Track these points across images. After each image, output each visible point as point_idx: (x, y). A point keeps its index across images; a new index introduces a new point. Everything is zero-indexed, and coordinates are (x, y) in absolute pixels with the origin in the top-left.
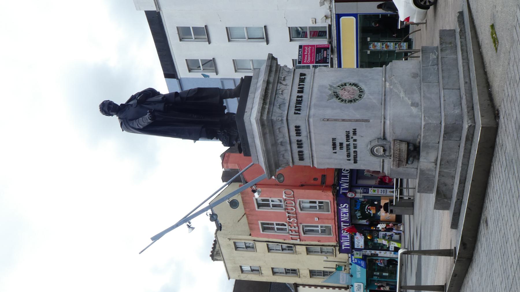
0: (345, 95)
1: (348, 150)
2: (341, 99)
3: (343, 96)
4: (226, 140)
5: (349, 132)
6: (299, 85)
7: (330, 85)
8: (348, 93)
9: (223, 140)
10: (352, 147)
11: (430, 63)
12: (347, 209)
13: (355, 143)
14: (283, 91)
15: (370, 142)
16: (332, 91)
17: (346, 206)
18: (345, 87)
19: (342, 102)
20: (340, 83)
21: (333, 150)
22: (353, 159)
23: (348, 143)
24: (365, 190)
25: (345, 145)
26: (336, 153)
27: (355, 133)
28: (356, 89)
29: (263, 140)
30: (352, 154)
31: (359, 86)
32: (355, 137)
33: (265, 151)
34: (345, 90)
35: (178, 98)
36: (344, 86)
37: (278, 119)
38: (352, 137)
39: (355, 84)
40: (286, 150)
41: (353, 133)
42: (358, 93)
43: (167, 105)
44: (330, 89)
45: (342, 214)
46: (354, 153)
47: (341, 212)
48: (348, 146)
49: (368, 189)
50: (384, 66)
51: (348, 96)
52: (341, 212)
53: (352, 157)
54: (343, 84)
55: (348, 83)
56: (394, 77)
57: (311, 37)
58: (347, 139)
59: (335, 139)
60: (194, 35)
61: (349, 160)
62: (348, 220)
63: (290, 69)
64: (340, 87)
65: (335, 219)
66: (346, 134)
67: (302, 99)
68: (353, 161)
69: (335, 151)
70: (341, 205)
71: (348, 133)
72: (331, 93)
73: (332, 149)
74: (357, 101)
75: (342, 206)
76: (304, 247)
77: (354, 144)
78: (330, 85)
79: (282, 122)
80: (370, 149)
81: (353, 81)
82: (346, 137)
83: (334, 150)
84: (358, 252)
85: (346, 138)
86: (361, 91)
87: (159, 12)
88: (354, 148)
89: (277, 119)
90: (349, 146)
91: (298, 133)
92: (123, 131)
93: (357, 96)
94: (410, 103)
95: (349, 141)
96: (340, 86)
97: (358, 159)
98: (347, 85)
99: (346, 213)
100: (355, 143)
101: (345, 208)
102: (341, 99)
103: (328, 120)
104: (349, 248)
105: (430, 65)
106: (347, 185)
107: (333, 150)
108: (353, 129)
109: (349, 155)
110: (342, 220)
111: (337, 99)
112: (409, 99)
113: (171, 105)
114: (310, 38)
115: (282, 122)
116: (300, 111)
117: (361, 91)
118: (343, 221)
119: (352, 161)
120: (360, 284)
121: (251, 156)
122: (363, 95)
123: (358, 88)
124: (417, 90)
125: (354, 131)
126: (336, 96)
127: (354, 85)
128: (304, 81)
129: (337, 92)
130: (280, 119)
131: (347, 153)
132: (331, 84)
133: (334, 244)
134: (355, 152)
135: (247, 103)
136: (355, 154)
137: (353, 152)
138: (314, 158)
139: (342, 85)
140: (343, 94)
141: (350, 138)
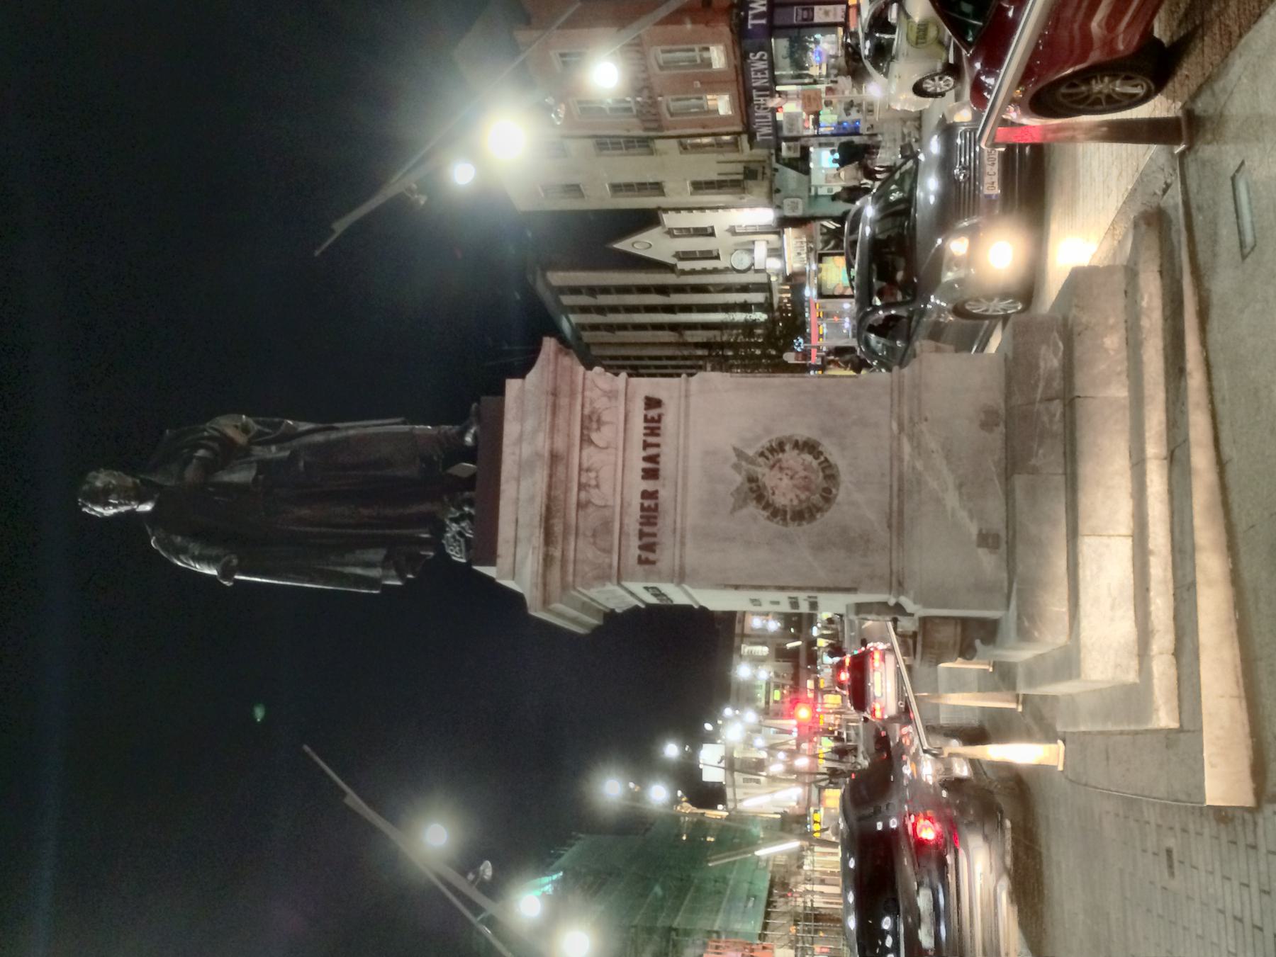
0: (784, 491)
3: (777, 492)
6: (646, 445)
7: (735, 449)
11: (1040, 390)
12: (766, 62)
16: (744, 473)
17: (763, 55)
18: (781, 455)
19: (775, 520)
20: (765, 442)
24: (805, 13)
28: (815, 463)
34: (781, 469)
36: (776, 451)
42: (819, 479)
44: (736, 467)
45: (753, 73)
47: (752, 69)
49: (813, 10)
51: (792, 495)
52: (752, 69)
54: (774, 445)
55: (789, 439)
56: (925, 423)
62: (767, 84)
65: (737, 80)
67: (657, 505)
70: (751, 55)
72: (742, 484)
75: (754, 56)
76: (674, 142)
78: (735, 449)
81: (802, 433)
84: (791, 144)
86: (829, 471)
93: (818, 496)
94: (973, 529)
96: (767, 453)
98: (787, 447)
99: (762, 72)
101: (761, 59)
104: (771, 137)
105: (1038, 397)
106: (764, 5)
110: (754, 85)
112: (971, 517)
116: (654, 551)
117: (828, 472)
118: (755, 88)
120: (796, 200)
122: (834, 491)
123: (819, 461)
124: (997, 482)
127: (806, 450)
128: (659, 428)
132: (739, 445)
133: (738, 128)
139: (772, 450)
140: (776, 487)
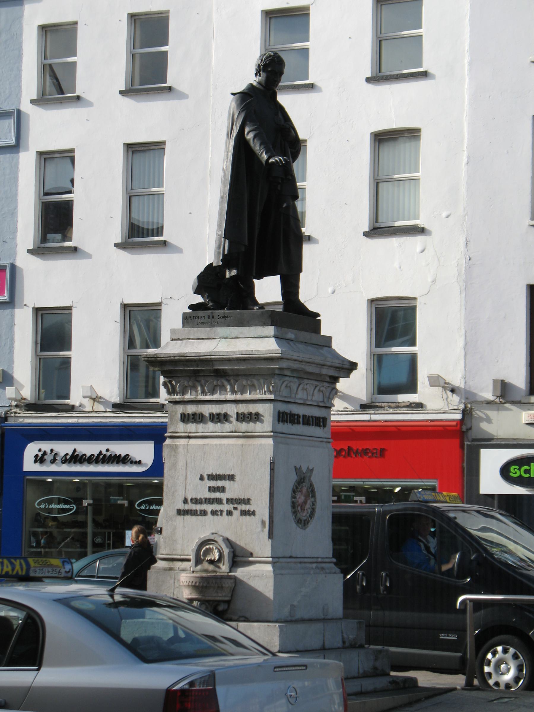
23: (225, 501)
25: (217, 495)
26: (202, 478)
27: (244, 513)
30: (198, 507)
32: (236, 513)
33: (210, 359)
48: (219, 501)
50: (334, 560)
55: (315, 501)
57: (129, 357)
60: (142, 54)
63: (332, 400)
64: (310, 487)
68: (182, 508)
69: (206, 477)
91: (242, 417)
97: (188, 518)
98: (313, 500)
102: (297, 490)
109: (196, 501)
114: (128, 356)
119: (181, 506)
122: (300, 526)
127: (312, 510)
134: (204, 513)
136: (199, 513)
141: (236, 506)
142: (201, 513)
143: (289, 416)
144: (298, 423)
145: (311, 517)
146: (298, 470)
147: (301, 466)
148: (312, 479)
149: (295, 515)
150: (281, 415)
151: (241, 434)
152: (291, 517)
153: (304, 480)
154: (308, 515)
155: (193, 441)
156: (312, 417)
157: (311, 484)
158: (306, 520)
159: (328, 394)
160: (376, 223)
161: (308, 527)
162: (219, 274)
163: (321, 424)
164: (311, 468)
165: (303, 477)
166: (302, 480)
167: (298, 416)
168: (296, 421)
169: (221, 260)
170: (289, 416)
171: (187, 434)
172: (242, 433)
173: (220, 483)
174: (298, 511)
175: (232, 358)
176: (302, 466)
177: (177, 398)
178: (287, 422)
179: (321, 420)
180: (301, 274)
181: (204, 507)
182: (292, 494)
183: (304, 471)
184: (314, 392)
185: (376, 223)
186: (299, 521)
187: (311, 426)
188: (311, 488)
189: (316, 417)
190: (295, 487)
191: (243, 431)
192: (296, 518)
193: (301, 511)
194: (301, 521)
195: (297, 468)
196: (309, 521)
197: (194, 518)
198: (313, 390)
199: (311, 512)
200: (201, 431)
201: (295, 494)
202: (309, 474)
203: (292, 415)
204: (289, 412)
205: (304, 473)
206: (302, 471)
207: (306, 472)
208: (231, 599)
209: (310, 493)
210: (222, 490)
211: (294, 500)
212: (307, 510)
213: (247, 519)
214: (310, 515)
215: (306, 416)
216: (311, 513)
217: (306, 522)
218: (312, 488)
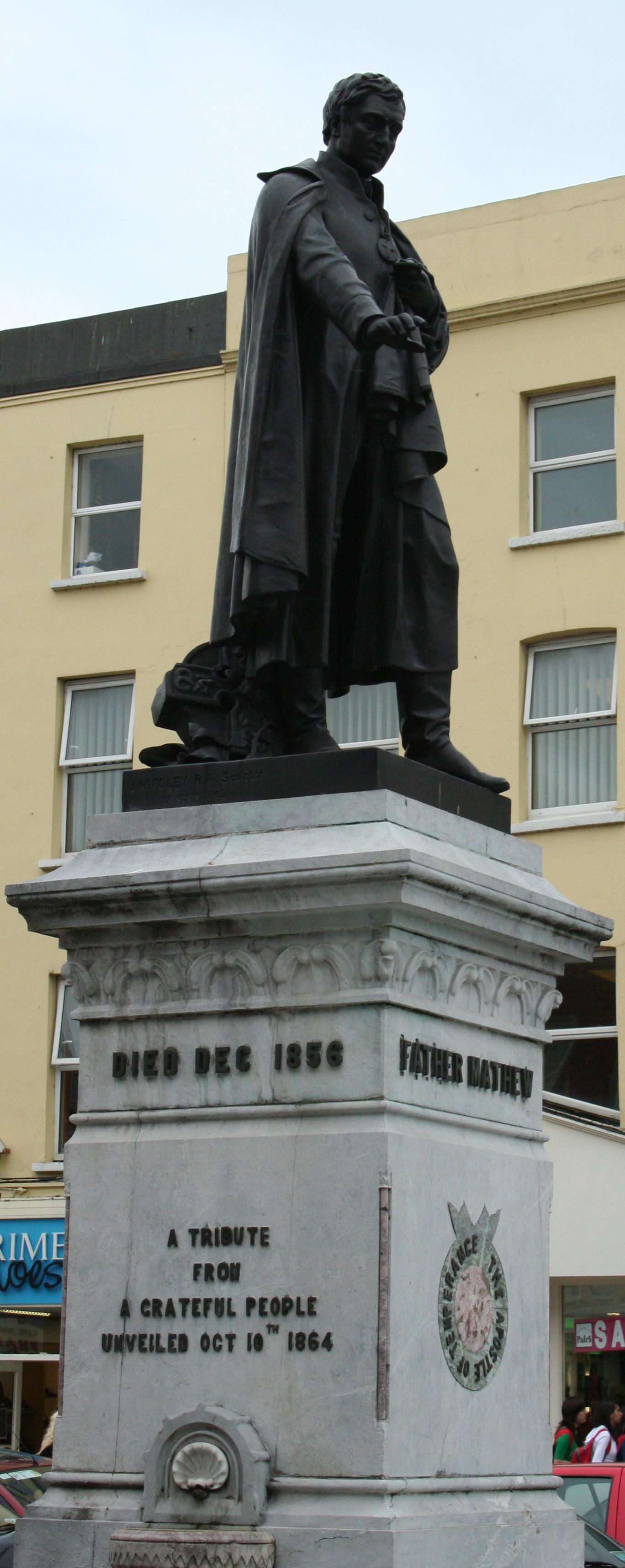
1: (195, 1308)
2: (452, 1275)
4: (197, 687)
5: (312, 1313)
8: (472, 1308)
9: (194, 669)
10: (212, 1325)
13: (241, 1343)
14: (519, 997)
15: (247, 1418)
18: (493, 1292)
21: (193, 1232)
22: (130, 1332)
23: (239, 1307)
25: (221, 1290)
26: (173, 1241)
29: (273, 881)
30: (164, 1328)
31: (494, 1361)
32: (275, 1344)
35: (417, 469)
37: (386, 961)
38: (281, 1329)
39: (502, 1341)
40: (184, 991)
41: (308, 1334)
43: (395, 408)
46: (172, 1337)
48: (222, 1308)
53: (137, 1325)
58: (263, 1301)
59: (264, 1244)
60: (93, 518)
61: (125, 1312)
66: (299, 1299)
69: (184, 1238)
71: (304, 1308)
73: (200, 1226)
74: (448, 1355)
77: (231, 1337)
79: (370, 980)
80: (215, 1417)
82: (275, 1300)
83: (189, 1238)
85: (270, 1298)
87: (219, 362)
88: (205, 1337)
89: (390, 957)
90: (219, 1314)
92: (264, 177)
95: (248, 1314)
97: (133, 1359)
98: (498, 1303)
100: (241, 1343)
102: (455, 1275)
103: (384, 1209)
107: (193, 1232)
108: (329, 1335)
111: (455, 1253)
113: (393, 429)
115: (370, 980)
119: (115, 1327)
121: (126, 807)
125: (320, 1339)
126: (463, 1247)
127: (497, 1334)
129: (475, 1252)
130: (388, 971)
131: (170, 1302)
134: (182, 1344)
135: (326, 795)
137: (177, 1331)
138: (132, 1129)
141: (271, 1320)
142: (171, 1344)
143: (430, 1054)
144: (457, 1078)
145: (495, 1357)
146: (456, 1217)
147: (464, 1205)
148: (494, 1242)
149: (451, 1347)
150: (409, 1050)
151: (291, 1108)
152: (441, 1354)
153: (474, 1245)
154: (487, 1348)
155: (149, 1135)
156: (494, 1065)
157: (493, 1258)
158: (482, 1363)
159: (533, 1005)
160: (533, 808)
161: (486, 1383)
162: (226, 672)
163: (518, 1087)
164: (492, 1211)
165: (470, 1238)
166: (470, 1246)
167: (457, 1059)
168: (450, 1072)
169: (233, 621)
170: (430, 1054)
171: (133, 1114)
172: (293, 1103)
173: (227, 1255)
174: (460, 1336)
175: (263, 882)
176: (468, 1205)
177: (104, 1010)
178: (425, 1073)
179: (518, 1076)
180: (454, 672)
181: (181, 1325)
182: (441, 1285)
183: (475, 1222)
184: (499, 993)
185: (533, 808)
186: (463, 1368)
187: (489, 1090)
188: (494, 1270)
189: (503, 1066)
190: (449, 1264)
191: (296, 1098)
192: (453, 1358)
193: (468, 1336)
194: (468, 1364)
195: (456, 1210)
196: (490, 1367)
197: (152, 1360)
198: (494, 988)
199: (495, 1340)
200: (174, 1103)
201: (451, 1287)
202: (487, 1230)
203: (440, 1055)
204: (430, 1044)
205: (472, 1225)
206: (469, 1219)
207: (478, 1222)
208: (253, 1426)
209: (492, 1284)
210: (231, 1273)
211: (446, 1302)
212: (482, 1332)
213: (304, 1359)
214: (492, 1349)
215: (477, 1060)
216: (494, 1343)
217: (481, 1368)
218: (497, 1270)
